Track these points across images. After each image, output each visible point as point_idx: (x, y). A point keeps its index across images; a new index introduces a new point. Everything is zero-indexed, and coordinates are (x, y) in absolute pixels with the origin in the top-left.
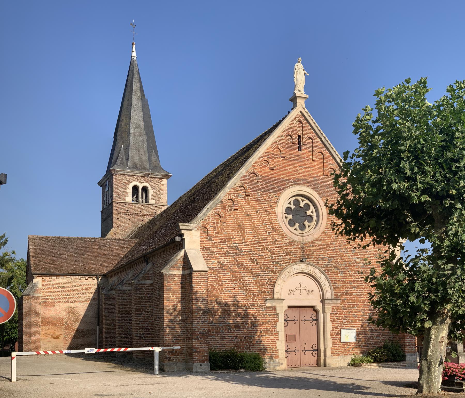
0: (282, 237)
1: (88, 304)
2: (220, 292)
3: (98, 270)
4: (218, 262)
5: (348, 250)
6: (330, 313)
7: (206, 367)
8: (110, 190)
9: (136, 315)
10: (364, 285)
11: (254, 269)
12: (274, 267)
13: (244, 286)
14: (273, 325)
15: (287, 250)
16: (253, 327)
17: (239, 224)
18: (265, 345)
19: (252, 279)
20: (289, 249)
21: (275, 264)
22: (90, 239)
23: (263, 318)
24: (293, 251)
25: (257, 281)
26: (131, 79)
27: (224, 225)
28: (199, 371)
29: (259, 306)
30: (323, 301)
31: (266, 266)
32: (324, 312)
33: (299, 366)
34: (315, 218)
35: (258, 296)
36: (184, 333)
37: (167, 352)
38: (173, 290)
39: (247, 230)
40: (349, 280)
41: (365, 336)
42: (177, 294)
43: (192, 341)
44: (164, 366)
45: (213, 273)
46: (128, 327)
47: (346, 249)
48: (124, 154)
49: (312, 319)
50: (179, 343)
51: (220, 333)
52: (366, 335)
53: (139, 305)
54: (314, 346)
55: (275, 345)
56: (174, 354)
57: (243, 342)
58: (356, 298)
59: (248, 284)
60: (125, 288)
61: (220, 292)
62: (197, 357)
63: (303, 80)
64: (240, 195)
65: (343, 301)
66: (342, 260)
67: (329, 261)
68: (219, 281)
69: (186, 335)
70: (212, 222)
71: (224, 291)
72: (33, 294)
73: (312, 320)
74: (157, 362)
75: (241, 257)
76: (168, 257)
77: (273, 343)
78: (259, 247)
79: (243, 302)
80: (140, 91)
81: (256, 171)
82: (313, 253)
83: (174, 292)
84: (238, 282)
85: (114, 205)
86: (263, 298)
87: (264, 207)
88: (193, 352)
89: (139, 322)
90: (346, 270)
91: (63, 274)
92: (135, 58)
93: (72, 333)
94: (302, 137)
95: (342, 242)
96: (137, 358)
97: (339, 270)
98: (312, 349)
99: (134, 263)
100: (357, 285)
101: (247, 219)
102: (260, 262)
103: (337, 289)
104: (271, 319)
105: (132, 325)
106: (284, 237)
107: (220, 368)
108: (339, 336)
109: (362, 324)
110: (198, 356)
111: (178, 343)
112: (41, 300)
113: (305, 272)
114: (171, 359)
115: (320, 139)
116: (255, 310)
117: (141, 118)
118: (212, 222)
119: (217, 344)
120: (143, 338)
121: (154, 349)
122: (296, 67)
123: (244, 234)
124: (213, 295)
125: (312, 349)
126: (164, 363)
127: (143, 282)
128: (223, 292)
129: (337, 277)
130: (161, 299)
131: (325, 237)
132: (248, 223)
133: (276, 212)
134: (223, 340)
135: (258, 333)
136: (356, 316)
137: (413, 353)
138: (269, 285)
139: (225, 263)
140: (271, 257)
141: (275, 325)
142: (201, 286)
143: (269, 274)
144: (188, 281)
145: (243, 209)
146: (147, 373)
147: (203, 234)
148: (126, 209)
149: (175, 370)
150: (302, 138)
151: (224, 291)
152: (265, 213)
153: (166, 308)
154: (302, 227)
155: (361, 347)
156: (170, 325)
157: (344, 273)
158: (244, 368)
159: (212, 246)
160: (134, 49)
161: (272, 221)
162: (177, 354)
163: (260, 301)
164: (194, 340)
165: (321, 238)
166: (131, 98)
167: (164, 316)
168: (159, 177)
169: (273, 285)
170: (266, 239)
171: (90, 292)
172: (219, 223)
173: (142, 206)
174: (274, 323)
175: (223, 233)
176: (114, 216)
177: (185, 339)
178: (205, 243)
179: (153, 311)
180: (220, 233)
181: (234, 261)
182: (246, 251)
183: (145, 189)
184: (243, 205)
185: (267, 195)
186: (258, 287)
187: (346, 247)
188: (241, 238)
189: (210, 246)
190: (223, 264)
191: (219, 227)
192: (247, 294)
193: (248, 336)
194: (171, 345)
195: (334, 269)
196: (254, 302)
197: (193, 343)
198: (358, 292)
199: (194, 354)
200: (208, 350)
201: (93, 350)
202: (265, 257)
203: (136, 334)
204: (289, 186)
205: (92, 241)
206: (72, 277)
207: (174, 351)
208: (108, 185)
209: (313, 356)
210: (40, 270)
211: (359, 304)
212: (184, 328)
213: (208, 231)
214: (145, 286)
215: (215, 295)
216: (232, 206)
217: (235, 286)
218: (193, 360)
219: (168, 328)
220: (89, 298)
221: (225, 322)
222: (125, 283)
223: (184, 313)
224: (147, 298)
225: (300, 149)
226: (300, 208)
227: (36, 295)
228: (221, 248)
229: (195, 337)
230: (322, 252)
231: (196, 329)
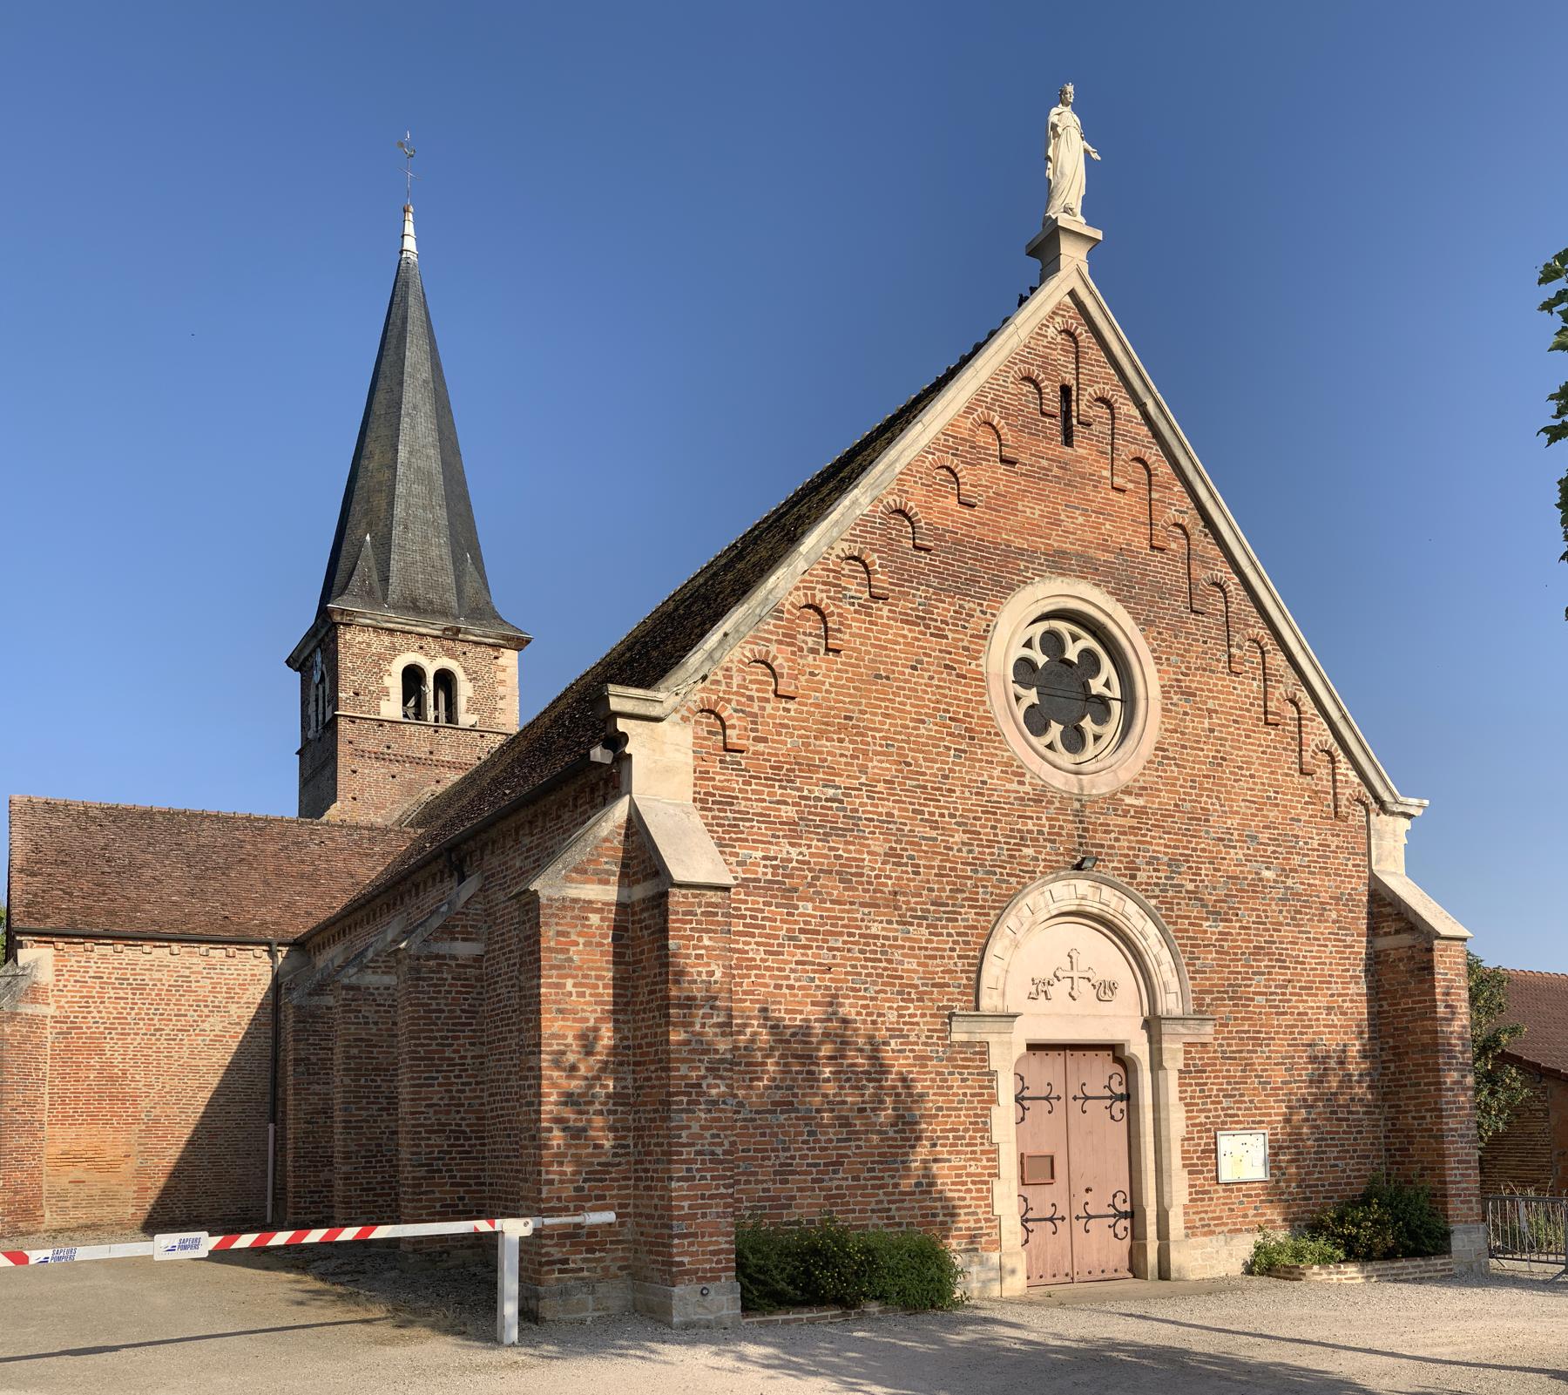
0: (1006, 772)
1: (235, 1046)
2: (772, 982)
3: (274, 924)
4: (765, 858)
5: (1236, 833)
6: (1180, 1071)
7: (725, 1300)
8: (327, 680)
9: (413, 1078)
10: (1289, 968)
11: (905, 894)
12: (977, 887)
13: (866, 959)
14: (976, 1115)
15: (1026, 824)
16: (903, 1123)
17: (847, 710)
18: (947, 1199)
19: (897, 930)
20: (1031, 818)
21: (980, 875)
22: (248, 819)
23: (939, 1087)
24: (1046, 830)
25: (915, 940)
26: (399, 322)
27: (788, 710)
28: (695, 1318)
29: (923, 1039)
30: (1154, 1024)
31: (948, 883)
32: (1157, 1064)
33: (1069, 1279)
34: (1116, 707)
35: (919, 1000)
36: (628, 1154)
37: (551, 1237)
38: (580, 968)
39: (877, 735)
40: (1241, 948)
41: (1297, 1160)
42: (596, 987)
43: (665, 1188)
44: (538, 1298)
45: (746, 902)
46: (383, 1126)
47: (1229, 831)
48: (372, 563)
49: (1108, 1093)
50: (603, 1197)
51: (773, 1150)
52: (1301, 1153)
53: (425, 1038)
54: (1120, 1197)
55: (986, 1198)
56: (584, 1243)
57: (865, 1187)
58: (1266, 1014)
59: (883, 953)
60: (371, 979)
61: (772, 982)
62: (686, 1259)
63: (1078, 178)
64: (848, 594)
65: (1221, 1025)
66: (1215, 869)
67: (1172, 872)
68: (768, 936)
69: (637, 1162)
70: (743, 695)
71: (788, 978)
72: (16, 1007)
73: (1111, 1098)
74: (510, 1284)
75: (852, 843)
76: (549, 844)
77: (978, 1191)
78: (920, 804)
79: (864, 1022)
80: (428, 365)
81: (910, 504)
82: (1117, 840)
83: (585, 976)
84: (845, 942)
85: (343, 725)
86: (939, 1008)
87: (941, 651)
88: (671, 1237)
89: (427, 1106)
90: (1230, 908)
91: (139, 935)
92: (414, 258)
93: (171, 1152)
94: (1074, 393)
95: (1212, 804)
96: (415, 1251)
97: (1207, 906)
98: (1112, 1211)
99: (409, 884)
100: (1266, 966)
101: (876, 691)
102: (925, 866)
103: (1202, 979)
104: (968, 1091)
105: (397, 1121)
106: (1015, 774)
107: (781, 1301)
108: (1210, 1158)
109: (1285, 1114)
110: (691, 1254)
111: (598, 1198)
112: (49, 1030)
113: (1089, 909)
114: (572, 1265)
115: (1141, 406)
116: (908, 1058)
117: (431, 452)
118: (743, 695)
119: (760, 1199)
120: (440, 1171)
121: (497, 1228)
122: (1053, 118)
123: (865, 753)
124: (745, 993)
125: (1112, 1211)
126: (540, 1284)
127: (444, 948)
128: (785, 983)
129: (1200, 932)
130: (529, 1004)
131: (1157, 783)
132: (880, 707)
133: (982, 674)
134: (787, 1182)
135: (923, 1151)
136: (1265, 1083)
137: (1472, 1222)
138: (960, 957)
139: (794, 864)
140: (965, 849)
141: (985, 1116)
142: (703, 952)
143: (960, 913)
144: (647, 927)
145: (859, 651)
146: (461, 1334)
147: (705, 739)
148: (381, 741)
149: (589, 1316)
150: (1074, 398)
151: (788, 978)
152: (944, 676)
153: (550, 1045)
154: (1075, 740)
155: (1287, 1201)
156: (567, 1120)
157: (1222, 920)
158: (877, 1298)
159: (741, 791)
160: (409, 228)
161: (968, 707)
162: (597, 1243)
163: (928, 1019)
164: (674, 1184)
165: (1142, 784)
166: (401, 383)
167: (540, 1077)
168: (491, 641)
169: (975, 957)
170: (946, 777)
171: (243, 1001)
172: (767, 700)
173: (436, 732)
174: (982, 1109)
175: (785, 743)
176: (341, 761)
177: (630, 1179)
178: (714, 779)
179: (482, 1063)
180: (774, 741)
181: (827, 857)
182: (871, 820)
183: (445, 680)
184: (860, 636)
185: (950, 604)
186: (919, 964)
187: (1229, 822)
188: (852, 765)
189: (733, 790)
190: (785, 868)
191: (770, 716)
192: (877, 992)
193: (881, 1163)
194: (571, 1205)
195: (1187, 905)
196: (905, 1023)
197: (671, 1199)
198: (1272, 994)
199: (677, 1246)
200: (732, 1225)
201: (195, 1244)
202: (945, 848)
203: (413, 1154)
204: (1029, 575)
205: (259, 826)
206: (175, 947)
207: (585, 1231)
208: (319, 664)
209: (1116, 1236)
210: (48, 916)
211: (1273, 1039)
212: (628, 1129)
213: (724, 727)
214: (453, 963)
215: (752, 993)
216: (816, 636)
217: (834, 957)
218: (670, 1272)
219: (556, 1133)
220: (239, 1024)
221: (791, 1103)
222: (372, 961)
223: (626, 1068)
224: (459, 1013)
225: (1068, 440)
226: (1065, 666)
227: (27, 1009)
228: (778, 802)
229: (679, 1170)
230: (1145, 835)
231: (684, 1133)
